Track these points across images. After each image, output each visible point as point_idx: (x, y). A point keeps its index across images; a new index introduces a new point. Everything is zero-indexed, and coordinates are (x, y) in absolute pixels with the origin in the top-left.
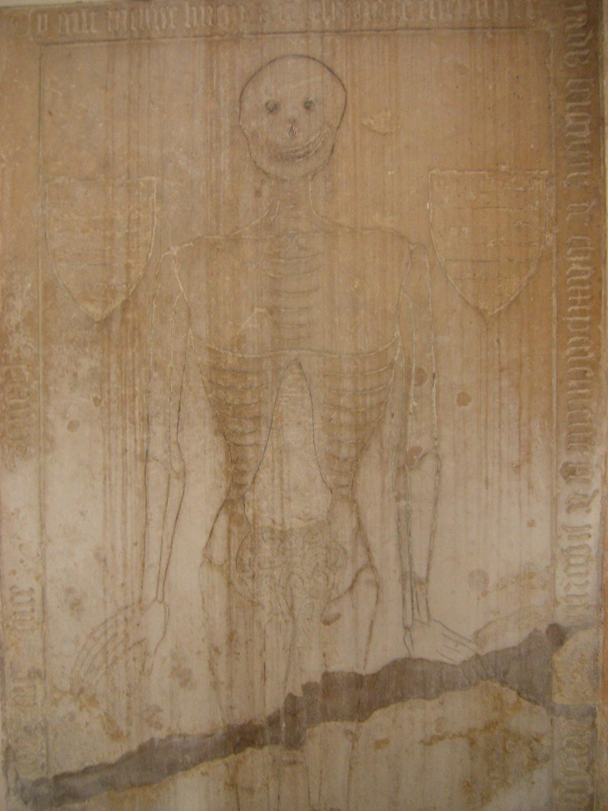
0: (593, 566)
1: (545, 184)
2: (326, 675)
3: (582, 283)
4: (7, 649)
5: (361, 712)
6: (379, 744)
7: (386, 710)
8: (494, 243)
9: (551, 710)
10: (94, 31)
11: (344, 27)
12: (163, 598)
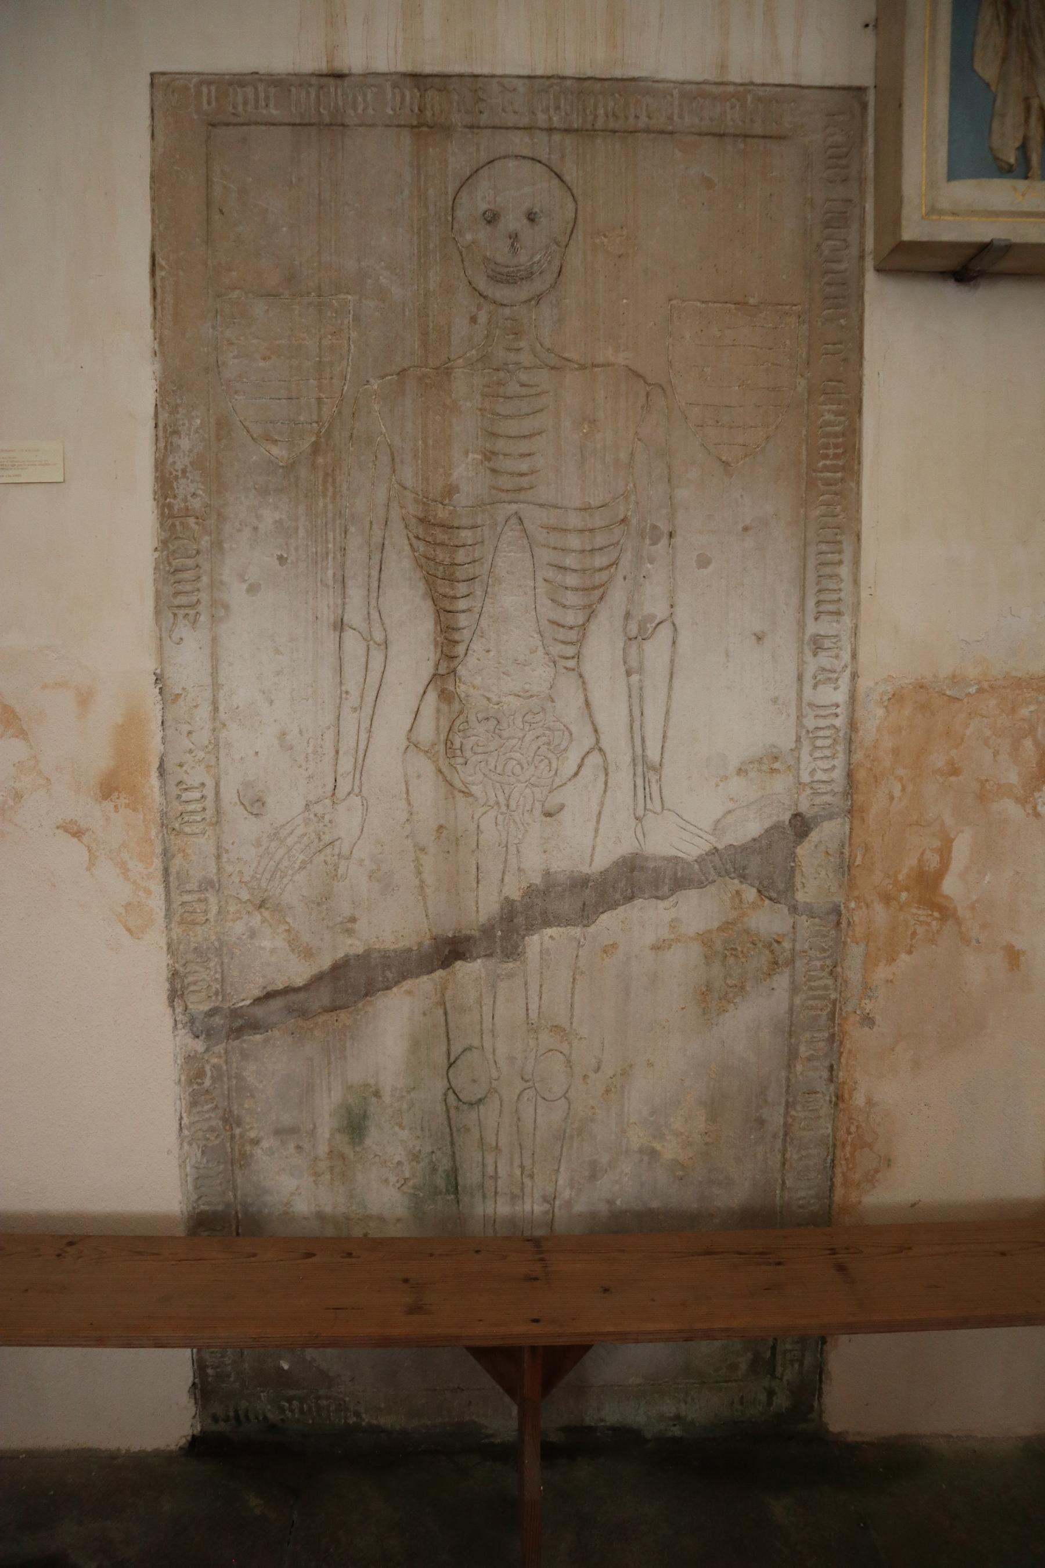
0: (840, 748)
2: (547, 873)
3: (836, 435)
4: (173, 856)
5: (586, 915)
6: (609, 949)
7: (615, 912)
8: (739, 386)
9: (794, 909)
10: (274, 112)
11: (576, 126)
12: (361, 791)
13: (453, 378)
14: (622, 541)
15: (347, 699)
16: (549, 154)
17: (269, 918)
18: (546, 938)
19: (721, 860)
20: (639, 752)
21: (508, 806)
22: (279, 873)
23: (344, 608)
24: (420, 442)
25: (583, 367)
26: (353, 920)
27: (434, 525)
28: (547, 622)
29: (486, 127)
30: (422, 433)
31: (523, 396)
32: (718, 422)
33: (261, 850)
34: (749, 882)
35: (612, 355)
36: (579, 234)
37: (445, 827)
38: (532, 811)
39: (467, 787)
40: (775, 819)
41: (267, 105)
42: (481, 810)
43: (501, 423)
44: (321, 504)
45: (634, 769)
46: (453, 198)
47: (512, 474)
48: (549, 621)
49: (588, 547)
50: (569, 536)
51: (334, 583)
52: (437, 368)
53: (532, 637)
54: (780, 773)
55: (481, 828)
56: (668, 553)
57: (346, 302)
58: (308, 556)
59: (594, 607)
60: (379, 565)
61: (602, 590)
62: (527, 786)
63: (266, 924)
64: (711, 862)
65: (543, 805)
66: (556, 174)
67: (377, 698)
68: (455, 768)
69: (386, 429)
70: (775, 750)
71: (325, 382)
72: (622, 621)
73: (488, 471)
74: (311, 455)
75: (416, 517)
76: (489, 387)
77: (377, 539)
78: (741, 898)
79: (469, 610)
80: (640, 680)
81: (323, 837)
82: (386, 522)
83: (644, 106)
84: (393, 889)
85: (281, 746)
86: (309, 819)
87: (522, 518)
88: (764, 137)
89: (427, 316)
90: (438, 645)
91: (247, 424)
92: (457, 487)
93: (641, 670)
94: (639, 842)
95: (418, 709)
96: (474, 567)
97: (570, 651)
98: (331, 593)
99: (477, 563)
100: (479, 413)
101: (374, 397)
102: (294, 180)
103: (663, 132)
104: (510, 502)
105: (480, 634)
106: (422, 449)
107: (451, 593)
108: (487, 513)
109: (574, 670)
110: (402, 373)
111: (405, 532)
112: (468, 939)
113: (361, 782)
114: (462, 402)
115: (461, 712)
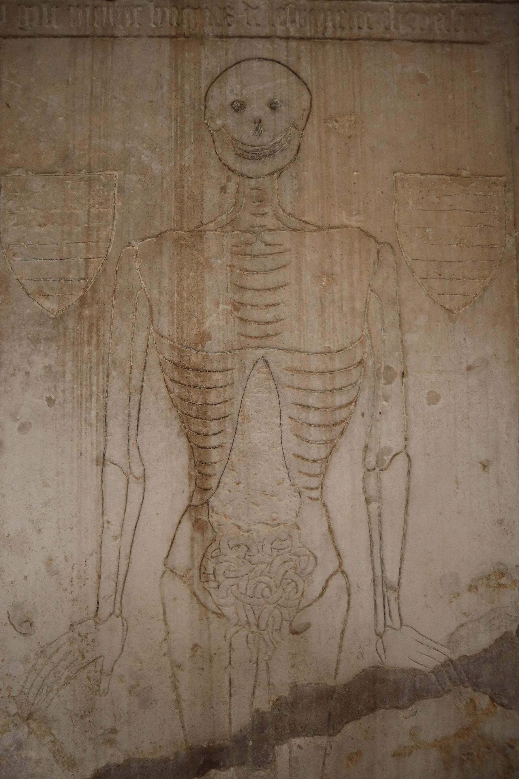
1: (504, 189)
2: (295, 687)
8: (457, 244)
10: (55, 27)
11: (309, 35)
12: (121, 613)
13: (205, 239)
14: (359, 382)
15: (108, 528)
16: (287, 56)
17: (36, 729)
18: (295, 747)
19: (455, 670)
20: (379, 573)
21: (258, 626)
22: (45, 688)
23: (106, 445)
24: (176, 295)
25: (320, 229)
26: (114, 731)
27: (188, 368)
28: (292, 456)
29: (234, 37)
30: (178, 287)
31: (268, 254)
32: (440, 275)
33: (29, 666)
34: (481, 690)
35: (346, 219)
36: (314, 120)
37: (199, 646)
38: (280, 630)
39: (219, 609)
40: (503, 630)
41: (49, 22)
42: (233, 630)
43: (249, 278)
44: (86, 352)
45: (375, 589)
46: (205, 92)
47: (258, 322)
48: (294, 455)
49: (329, 387)
50: (311, 377)
51: (97, 422)
52: (192, 231)
53: (279, 470)
54: (507, 587)
55: (233, 646)
56: (401, 391)
57: (112, 177)
58: (74, 398)
59: (336, 441)
60: (137, 406)
61: (342, 426)
62: (275, 607)
63: (33, 735)
64: (447, 672)
65: (291, 624)
66: (293, 72)
67: (136, 527)
68: (209, 591)
69: (146, 284)
70: (502, 567)
71: (92, 244)
72: (362, 454)
73: (237, 320)
74: (78, 307)
75: (171, 362)
76: (237, 246)
77: (136, 382)
78: (475, 705)
79: (221, 446)
80: (379, 507)
81: (86, 654)
82: (145, 366)
83: (366, 19)
84: (152, 703)
85: (48, 571)
86: (74, 639)
87: (269, 361)
88: (467, 43)
89: (183, 187)
90: (191, 478)
91: (23, 281)
92: (209, 334)
93: (379, 498)
94: (380, 657)
95: (174, 537)
96: (225, 406)
97: (314, 482)
98: (94, 432)
99: (227, 403)
100: (228, 269)
101: (135, 257)
102: (70, 79)
103: (382, 39)
104: (257, 348)
105: (231, 468)
106: (177, 302)
107: (204, 431)
108: (236, 358)
109: (317, 499)
110: (160, 235)
111: (161, 375)
112: (222, 749)
113: (121, 604)
114: (213, 260)
115: (214, 540)
